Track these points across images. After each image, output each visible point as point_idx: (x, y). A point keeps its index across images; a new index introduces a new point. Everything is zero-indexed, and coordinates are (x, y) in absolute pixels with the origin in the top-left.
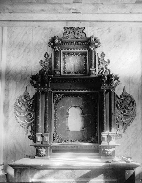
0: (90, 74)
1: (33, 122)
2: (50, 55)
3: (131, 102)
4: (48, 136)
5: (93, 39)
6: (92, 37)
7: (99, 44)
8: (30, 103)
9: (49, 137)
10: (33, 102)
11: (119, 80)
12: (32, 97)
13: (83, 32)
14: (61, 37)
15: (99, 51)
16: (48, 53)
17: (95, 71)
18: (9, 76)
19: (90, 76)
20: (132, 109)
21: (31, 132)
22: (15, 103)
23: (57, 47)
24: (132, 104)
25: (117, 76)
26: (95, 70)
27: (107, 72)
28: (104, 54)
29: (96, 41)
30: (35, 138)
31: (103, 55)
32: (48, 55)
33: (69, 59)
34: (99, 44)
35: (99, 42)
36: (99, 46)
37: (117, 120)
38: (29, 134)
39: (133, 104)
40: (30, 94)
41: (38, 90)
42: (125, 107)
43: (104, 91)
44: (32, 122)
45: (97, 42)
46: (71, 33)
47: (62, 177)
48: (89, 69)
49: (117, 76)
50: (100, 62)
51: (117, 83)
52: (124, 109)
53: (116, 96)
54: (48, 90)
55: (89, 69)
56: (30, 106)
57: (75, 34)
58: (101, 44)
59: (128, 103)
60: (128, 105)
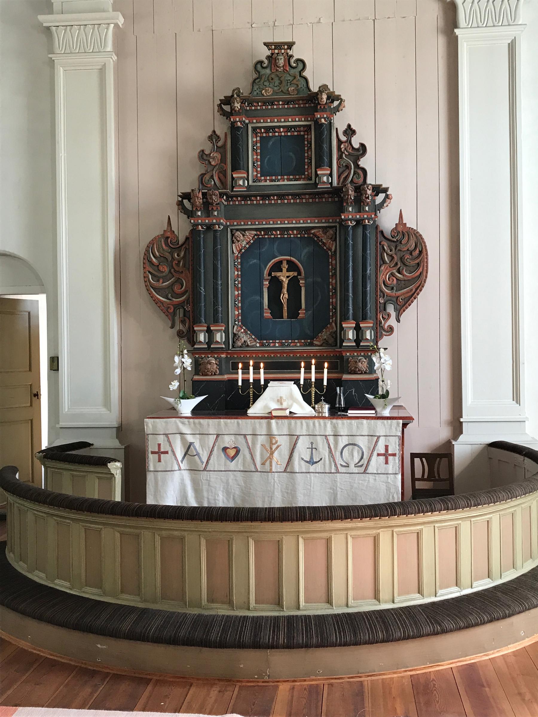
0: (318, 184)
1: (188, 299)
2: (222, 137)
3: (416, 246)
4: (222, 330)
5: (325, 97)
6: (324, 88)
7: (340, 104)
8: (178, 255)
9: (224, 334)
10: (185, 253)
11: (388, 193)
12: (182, 239)
13: (300, 76)
14: (245, 91)
15: (340, 122)
16: (218, 133)
17: (331, 175)
18: (532, 714)
19: (316, 188)
20: (418, 265)
21: (183, 322)
22: (145, 254)
23: (238, 119)
24: (417, 251)
25: (382, 185)
26: (329, 172)
27: (359, 175)
28: (351, 129)
29: (333, 97)
30: (193, 336)
31: (350, 131)
32: (218, 137)
33: (283, 501)
34: (340, 104)
35: (341, 99)
36: (340, 108)
37: (381, 291)
38: (179, 326)
39: (421, 252)
40: (175, 228)
41: (197, 225)
42: (401, 258)
43: (350, 224)
44: (185, 299)
45: (338, 98)
46: (272, 79)
47: (334, 262)
48: (316, 172)
49: (382, 185)
50: (343, 150)
51: (384, 201)
52: (399, 266)
53: (379, 235)
54: (219, 225)
55: (316, 172)
56: (179, 262)
57: (281, 83)
58: (346, 103)
59: (408, 250)
60: (407, 256)
